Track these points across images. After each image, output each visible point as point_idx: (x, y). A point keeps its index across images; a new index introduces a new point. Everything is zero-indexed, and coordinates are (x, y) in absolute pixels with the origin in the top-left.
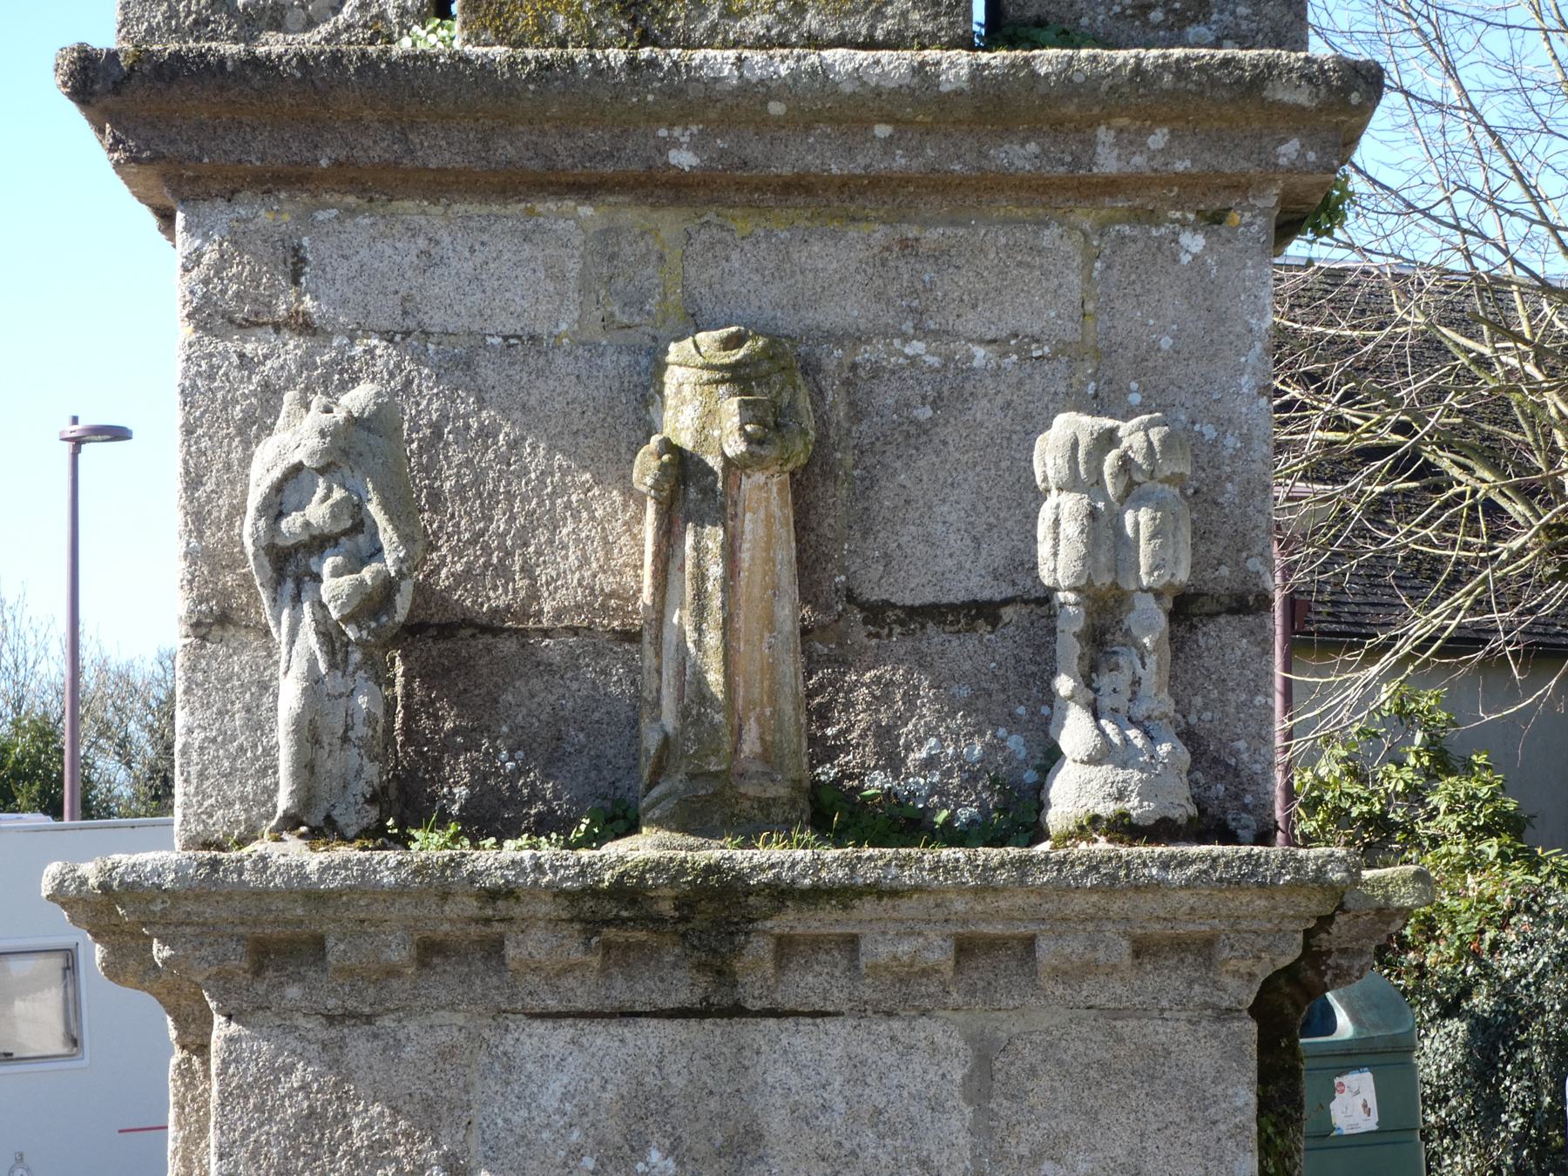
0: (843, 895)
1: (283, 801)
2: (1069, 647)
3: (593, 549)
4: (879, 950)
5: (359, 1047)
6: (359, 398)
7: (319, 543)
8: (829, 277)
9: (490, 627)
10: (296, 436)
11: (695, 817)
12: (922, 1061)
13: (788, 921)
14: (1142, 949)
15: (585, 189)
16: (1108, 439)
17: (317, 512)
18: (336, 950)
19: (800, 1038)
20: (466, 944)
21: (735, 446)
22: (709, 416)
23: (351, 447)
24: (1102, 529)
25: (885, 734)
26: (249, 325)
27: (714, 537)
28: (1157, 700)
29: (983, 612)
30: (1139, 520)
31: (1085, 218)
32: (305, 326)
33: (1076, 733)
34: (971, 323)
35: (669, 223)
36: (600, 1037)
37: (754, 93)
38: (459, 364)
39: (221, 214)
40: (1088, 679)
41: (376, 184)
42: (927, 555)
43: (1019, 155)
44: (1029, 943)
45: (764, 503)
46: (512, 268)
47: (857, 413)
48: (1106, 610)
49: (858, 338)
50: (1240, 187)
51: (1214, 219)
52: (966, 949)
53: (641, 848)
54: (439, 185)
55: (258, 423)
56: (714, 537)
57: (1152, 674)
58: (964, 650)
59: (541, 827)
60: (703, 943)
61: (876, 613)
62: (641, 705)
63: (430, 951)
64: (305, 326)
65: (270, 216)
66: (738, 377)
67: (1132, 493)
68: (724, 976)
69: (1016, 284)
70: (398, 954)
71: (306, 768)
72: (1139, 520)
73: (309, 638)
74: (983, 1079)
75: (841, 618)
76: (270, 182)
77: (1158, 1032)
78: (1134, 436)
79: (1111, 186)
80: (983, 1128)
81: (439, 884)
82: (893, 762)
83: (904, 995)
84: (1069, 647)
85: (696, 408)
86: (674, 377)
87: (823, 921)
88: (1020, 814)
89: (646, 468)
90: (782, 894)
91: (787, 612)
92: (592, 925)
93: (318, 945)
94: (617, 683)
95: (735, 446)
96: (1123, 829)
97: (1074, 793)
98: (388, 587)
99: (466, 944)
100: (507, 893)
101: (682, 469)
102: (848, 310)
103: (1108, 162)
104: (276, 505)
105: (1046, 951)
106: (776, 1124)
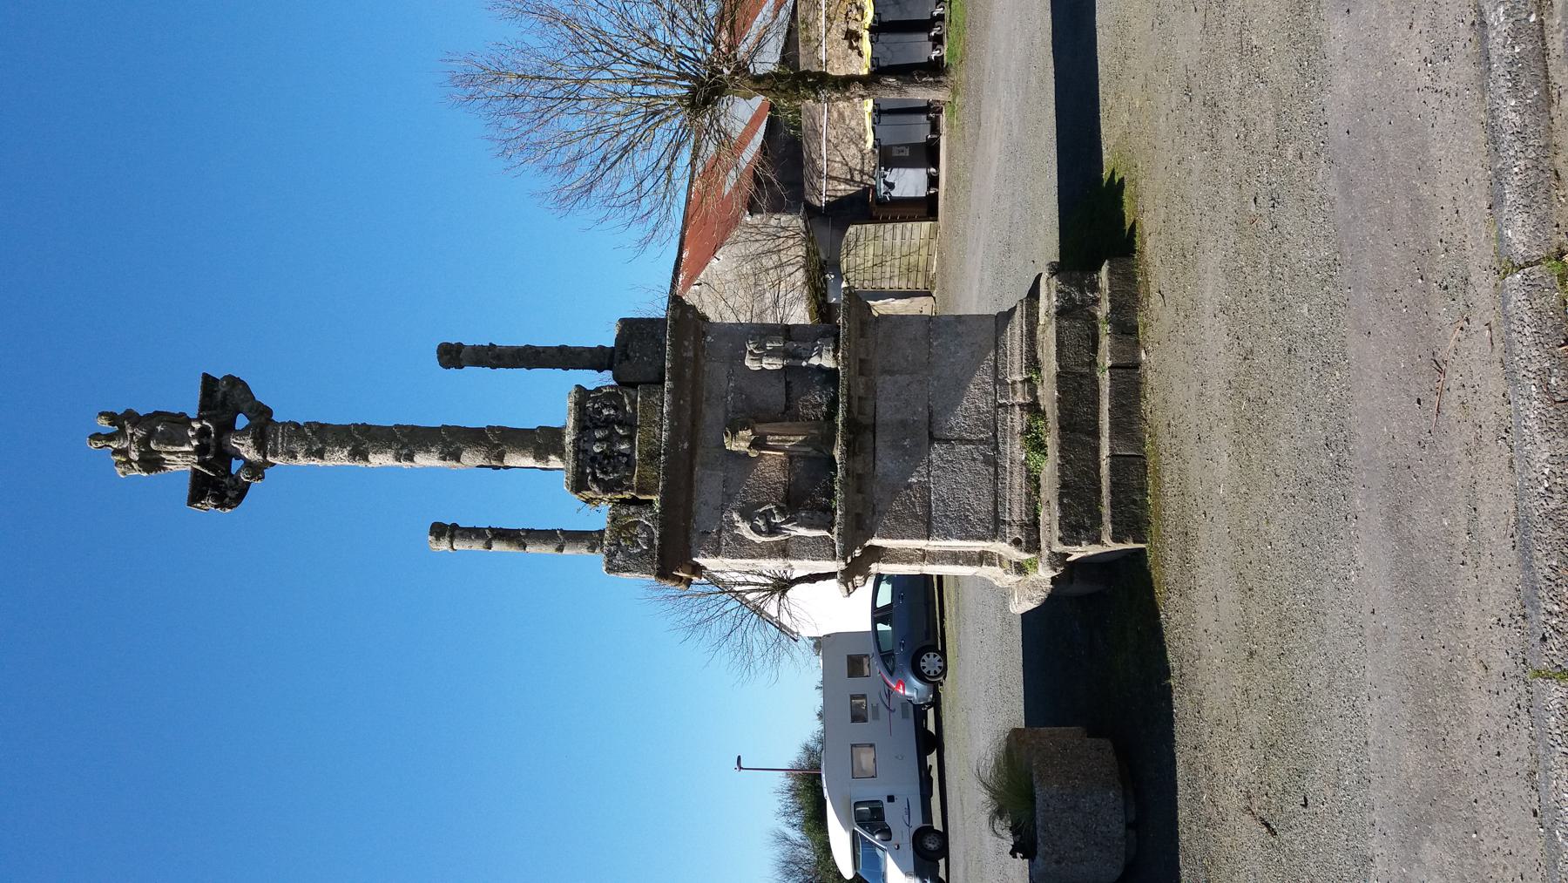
0: (849, 397)
1: (825, 533)
2: (796, 362)
3: (772, 465)
4: (861, 392)
5: (880, 508)
6: (736, 516)
7: (768, 523)
8: (712, 415)
9: (787, 492)
10: (744, 529)
11: (831, 443)
12: (885, 384)
13: (855, 410)
14: (862, 336)
15: (692, 469)
16: (751, 353)
17: (761, 523)
18: (859, 510)
19: (880, 411)
20: (858, 482)
21: (749, 432)
22: (743, 439)
23: (747, 516)
24: (771, 354)
25: (814, 407)
26: (719, 543)
27: (770, 438)
28: (808, 345)
29: (788, 384)
30: (769, 346)
31: (703, 361)
32: (719, 531)
33: (815, 361)
34: (724, 386)
35: (700, 451)
36: (879, 454)
37: (672, 428)
38: (729, 498)
39: (694, 548)
40: (803, 359)
41: (689, 515)
42: (775, 395)
43: (688, 373)
44: (861, 361)
45: (760, 428)
46: (709, 486)
47: (743, 411)
48: (785, 354)
49: (727, 412)
50: (697, 328)
51: (705, 334)
52: (861, 374)
53: (837, 454)
54: (690, 501)
55: (740, 540)
56: (770, 438)
57: (802, 345)
58: (796, 388)
59: (832, 482)
60: (860, 432)
61: (787, 408)
62: (805, 457)
63: (859, 491)
64: (719, 531)
65: (695, 539)
66: (734, 433)
67: (764, 347)
68: (866, 427)
69: (717, 376)
70: (860, 497)
71: (818, 527)
72: (769, 346)
73: (789, 526)
74: (891, 373)
75: (788, 414)
76: (688, 538)
77: (881, 335)
78: (750, 347)
79: (696, 355)
80: (900, 372)
81: (844, 485)
82: (821, 405)
83: (871, 389)
84: (796, 362)
85: (739, 444)
86: (734, 448)
87: (855, 403)
88: (831, 374)
89: (753, 454)
90: (849, 411)
91: (787, 424)
92: (854, 454)
93: (858, 515)
94: (801, 464)
95: (749, 432)
96: (836, 350)
97: (827, 362)
98: (778, 508)
99: (858, 482)
100: (847, 471)
101: (753, 445)
102: (721, 412)
103: (690, 354)
104: (758, 531)
105: (863, 356)
106: (899, 417)
